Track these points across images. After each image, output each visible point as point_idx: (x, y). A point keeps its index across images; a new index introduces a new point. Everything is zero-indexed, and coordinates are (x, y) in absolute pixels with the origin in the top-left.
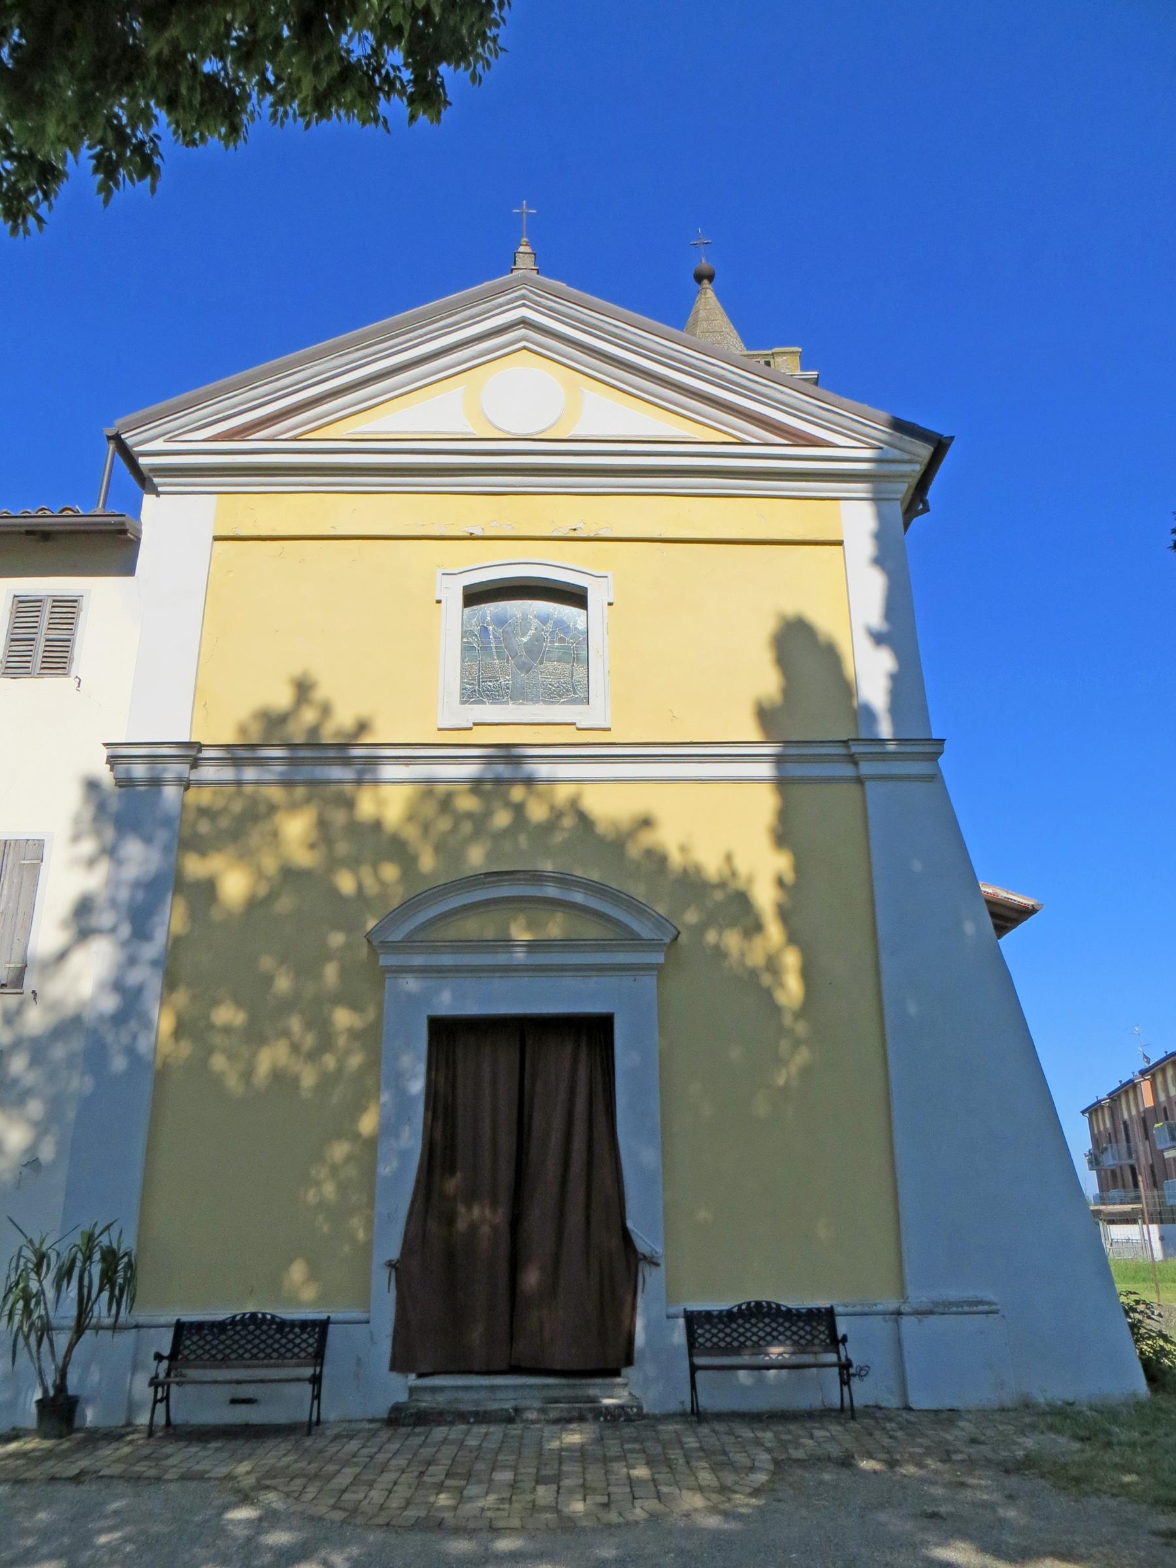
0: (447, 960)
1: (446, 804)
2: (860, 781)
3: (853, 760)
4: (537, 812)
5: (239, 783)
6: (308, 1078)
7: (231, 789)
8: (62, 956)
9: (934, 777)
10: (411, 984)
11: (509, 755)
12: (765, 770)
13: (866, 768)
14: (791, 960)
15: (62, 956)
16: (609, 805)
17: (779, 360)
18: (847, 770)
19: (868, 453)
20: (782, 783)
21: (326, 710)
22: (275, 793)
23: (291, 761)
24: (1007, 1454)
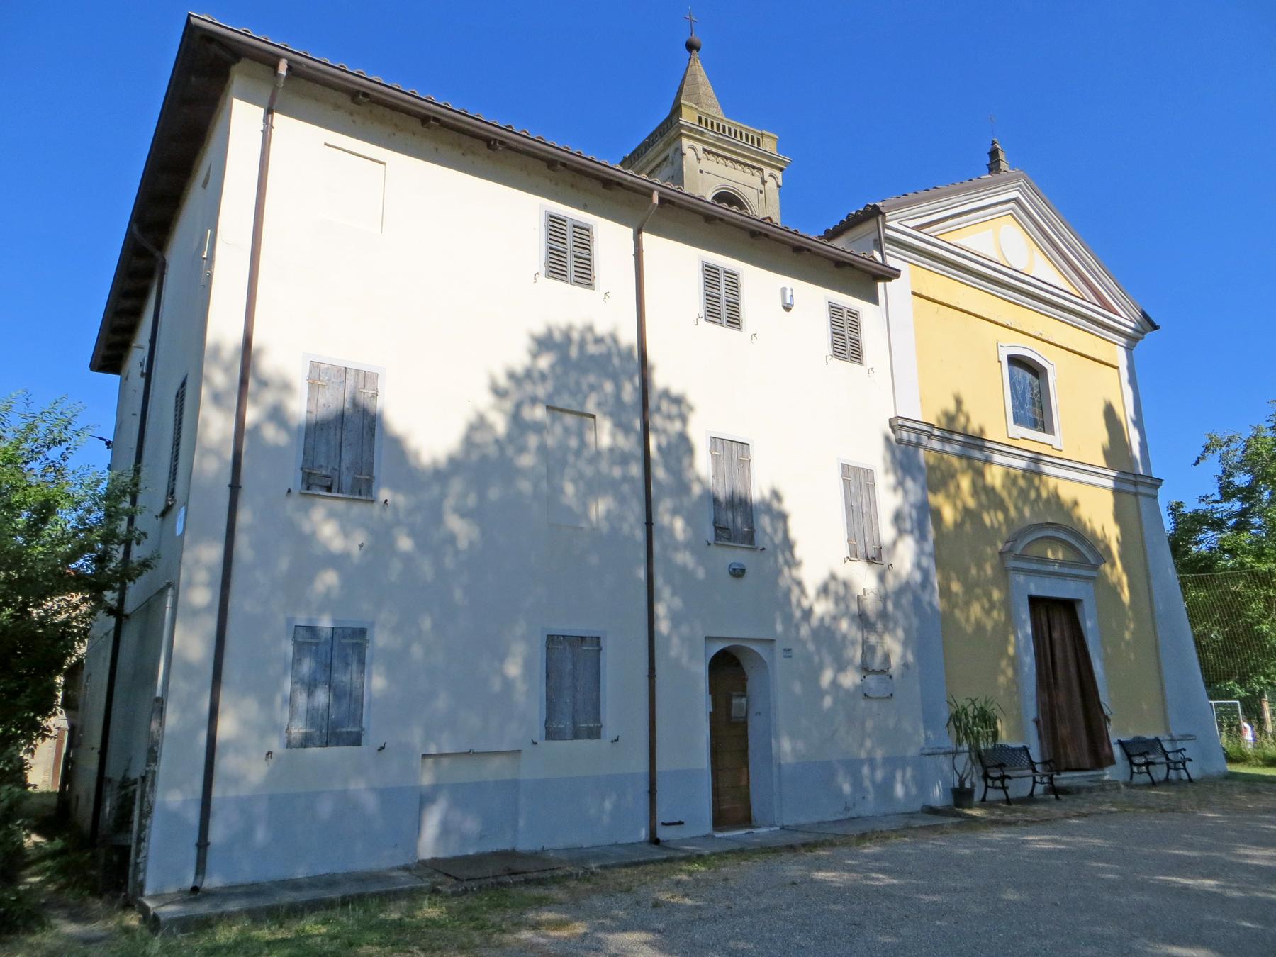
0: (1034, 566)
1: (1014, 481)
2: (1136, 494)
3: (1135, 484)
4: (1044, 494)
5: (942, 452)
6: (989, 626)
7: (938, 455)
8: (895, 543)
9: (1155, 497)
10: (1021, 578)
11: (1036, 459)
12: (1110, 483)
13: (1141, 489)
14: (1125, 580)
15: (895, 543)
16: (1067, 492)
17: (766, 140)
18: (1132, 489)
19: (1132, 325)
20: (1116, 491)
21: (968, 419)
22: (956, 462)
23: (964, 444)
24: (925, 846)
